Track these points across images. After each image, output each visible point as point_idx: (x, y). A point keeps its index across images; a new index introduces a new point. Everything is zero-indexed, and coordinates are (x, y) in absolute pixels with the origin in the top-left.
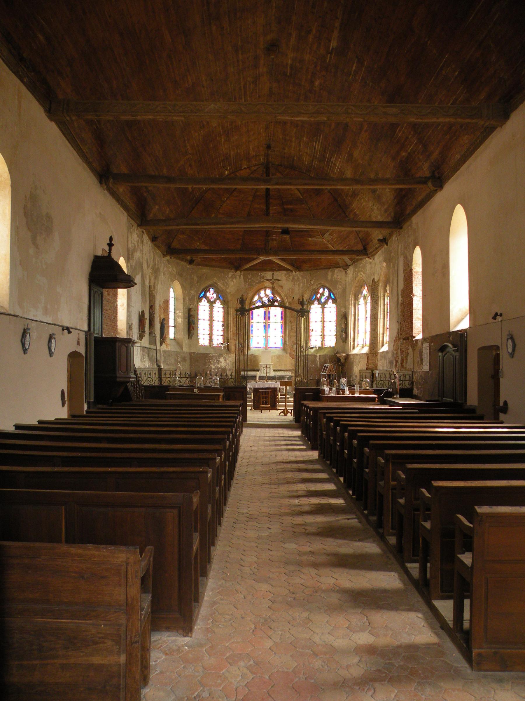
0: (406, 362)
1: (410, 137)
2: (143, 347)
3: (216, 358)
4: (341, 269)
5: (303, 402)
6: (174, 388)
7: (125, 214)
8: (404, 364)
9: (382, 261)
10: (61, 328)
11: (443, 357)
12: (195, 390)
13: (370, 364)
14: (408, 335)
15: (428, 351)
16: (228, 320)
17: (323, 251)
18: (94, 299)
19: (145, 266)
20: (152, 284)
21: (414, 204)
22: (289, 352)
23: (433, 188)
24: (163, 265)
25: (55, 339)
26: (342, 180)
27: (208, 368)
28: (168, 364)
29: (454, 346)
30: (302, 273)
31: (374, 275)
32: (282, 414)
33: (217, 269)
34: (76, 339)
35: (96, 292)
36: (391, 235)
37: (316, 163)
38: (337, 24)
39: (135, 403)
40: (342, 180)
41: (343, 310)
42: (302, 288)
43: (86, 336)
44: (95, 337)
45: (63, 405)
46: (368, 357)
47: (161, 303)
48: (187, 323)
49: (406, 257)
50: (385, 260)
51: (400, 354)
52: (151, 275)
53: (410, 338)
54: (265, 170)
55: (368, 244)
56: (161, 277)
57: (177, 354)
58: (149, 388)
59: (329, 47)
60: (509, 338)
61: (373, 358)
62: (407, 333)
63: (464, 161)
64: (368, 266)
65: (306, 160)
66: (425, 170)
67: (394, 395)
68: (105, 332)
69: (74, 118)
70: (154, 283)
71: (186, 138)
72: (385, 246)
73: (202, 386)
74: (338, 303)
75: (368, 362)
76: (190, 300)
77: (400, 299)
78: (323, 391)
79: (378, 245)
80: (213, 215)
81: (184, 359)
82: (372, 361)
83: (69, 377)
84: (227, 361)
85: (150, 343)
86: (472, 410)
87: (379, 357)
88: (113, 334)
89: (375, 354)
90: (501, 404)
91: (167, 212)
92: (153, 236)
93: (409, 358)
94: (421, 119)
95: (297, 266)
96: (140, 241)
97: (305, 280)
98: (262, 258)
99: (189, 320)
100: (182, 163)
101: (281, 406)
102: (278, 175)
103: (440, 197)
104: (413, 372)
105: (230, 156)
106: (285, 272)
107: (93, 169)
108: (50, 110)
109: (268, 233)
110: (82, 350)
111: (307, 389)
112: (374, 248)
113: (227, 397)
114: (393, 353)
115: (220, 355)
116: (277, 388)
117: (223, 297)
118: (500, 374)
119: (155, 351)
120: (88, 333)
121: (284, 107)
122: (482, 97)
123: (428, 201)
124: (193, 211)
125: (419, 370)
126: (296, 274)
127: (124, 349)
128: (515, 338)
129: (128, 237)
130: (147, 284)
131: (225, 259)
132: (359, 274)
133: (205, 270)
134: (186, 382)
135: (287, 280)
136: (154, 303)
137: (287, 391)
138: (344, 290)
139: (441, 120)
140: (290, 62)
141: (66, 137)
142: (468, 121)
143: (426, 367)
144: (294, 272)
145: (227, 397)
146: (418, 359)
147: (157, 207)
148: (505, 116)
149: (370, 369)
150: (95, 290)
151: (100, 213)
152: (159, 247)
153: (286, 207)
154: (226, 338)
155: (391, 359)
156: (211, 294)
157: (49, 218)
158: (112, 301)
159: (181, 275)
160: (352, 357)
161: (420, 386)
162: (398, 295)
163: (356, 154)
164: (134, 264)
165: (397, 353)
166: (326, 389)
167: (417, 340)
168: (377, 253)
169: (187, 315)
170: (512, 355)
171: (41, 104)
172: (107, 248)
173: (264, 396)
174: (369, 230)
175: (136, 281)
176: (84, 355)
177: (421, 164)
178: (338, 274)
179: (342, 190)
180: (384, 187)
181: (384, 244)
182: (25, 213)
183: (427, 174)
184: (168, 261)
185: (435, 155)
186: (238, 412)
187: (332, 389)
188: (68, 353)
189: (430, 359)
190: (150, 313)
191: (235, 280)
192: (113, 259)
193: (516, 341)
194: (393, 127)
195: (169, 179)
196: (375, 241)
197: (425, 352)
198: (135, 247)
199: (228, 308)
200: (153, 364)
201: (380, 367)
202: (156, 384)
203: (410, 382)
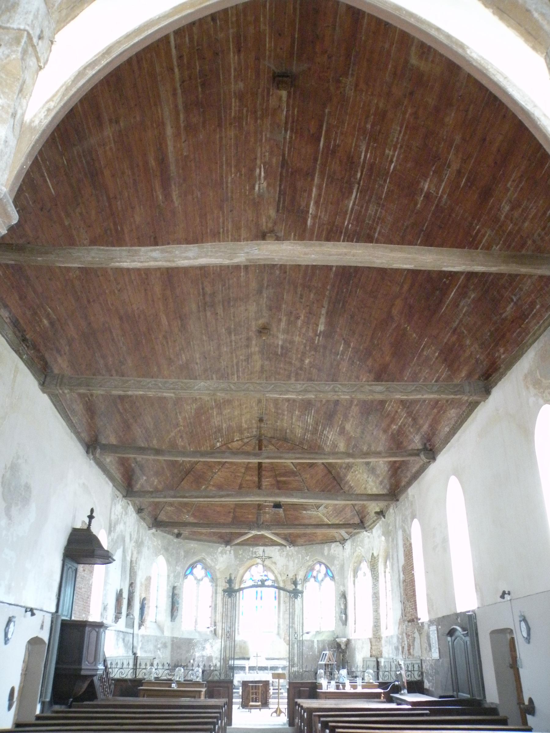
0: (413, 648)
1: (399, 410)
2: (118, 631)
3: (201, 644)
4: (338, 543)
5: (297, 700)
6: (150, 683)
7: (111, 484)
8: (411, 651)
9: (381, 535)
10: (24, 609)
11: (453, 642)
12: (174, 685)
13: (374, 651)
14: (413, 617)
15: (436, 635)
16: (216, 600)
17: (318, 525)
18: (67, 578)
19: (127, 539)
20: (134, 559)
21: (409, 476)
22: (283, 637)
23: (426, 460)
24: (148, 538)
25: (14, 622)
26: (334, 453)
27: (191, 655)
28: (145, 652)
29: (464, 629)
30: (296, 548)
31: (373, 550)
32: (275, 714)
33: (206, 543)
34: (40, 622)
35: (70, 567)
36: (388, 507)
37: (308, 436)
38: (324, 311)
39: (99, 703)
40: (334, 453)
41: (342, 588)
42: (297, 564)
43: (52, 618)
44: (63, 620)
45: (10, 708)
46: (371, 642)
47: (143, 580)
48: (170, 604)
49: (404, 531)
50: (384, 534)
51: (405, 638)
52: (133, 549)
53: (415, 620)
54: (257, 442)
55: (365, 516)
56: (145, 551)
57: (157, 639)
58: (120, 682)
59: (317, 331)
60: (521, 619)
61: (377, 644)
62: (412, 615)
63: (454, 434)
64: (366, 540)
65: (299, 432)
66: (416, 442)
67: (401, 690)
68: (75, 614)
69: (66, 391)
70: (137, 558)
71: (177, 411)
72: (383, 519)
73: (182, 680)
74: (336, 581)
75: (371, 648)
76: (175, 577)
77: (402, 575)
78: (320, 686)
79: (375, 518)
80: (203, 487)
81: (165, 646)
82: (376, 647)
83: (25, 669)
84: (214, 647)
85: (127, 626)
86: (493, 711)
87: (383, 642)
88: (84, 616)
89: (379, 638)
90: (526, 702)
91: (155, 483)
92: (139, 507)
93: (416, 644)
94: (407, 396)
95: (292, 541)
96: (124, 512)
97: (300, 556)
98: (254, 532)
99: (172, 599)
100: (173, 434)
101: (273, 704)
102: (271, 447)
103: (433, 469)
104: (421, 660)
105: (222, 429)
106: (278, 547)
107: (81, 440)
108: (44, 383)
109: (259, 507)
110: (45, 636)
111: (302, 683)
112: (371, 521)
113: (210, 694)
114: (398, 638)
115: (206, 640)
116: (269, 681)
117: (212, 575)
118: (519, 663)
119: (131, 636)
120: (55, 615)
121: (273, 386)
122: (463, 374)
123: (423, 472)
124: (183, 483)
125: (428, 658)
126: (291, 550)
127: (94, 634)
128: (527, 619)
129: (111, 509)
130: (128, 559)
131: (214, 533)
132: (357, 549)
133: (193, 545)
134: (163, 674)
135: (280, 555)
136: (135, 580)
137: (280, 684)
138: (342, 567)
139: (425, 396)
140: (280, 343)
141: (56, 408)
142: (452, 396)
143: (435, 655)
144: (288, 547)
145: (210, 694)
146: (425, 645)
147: (145, 478)
148: (487, 392)
149: (374, 656)
150: (70, 565)
151: (84, 484)
152: (144, 519)
153: (279, 479)
154: (213, 621)
155: (396, 645)
156: (199, 571)
157: (27, 487)
158: (87, 578)
159: (167, 550)
160: (353, 642)
161: (431, 678)
162: (399, 571)
163: (348, 427)
164: (115, 538)
165: (402, 638)
166: (323, 682)
167: (422, 623)
168: (374, 526)
169: (171, 594)
170: (528, 640)
171: (36, 378)
172: (87, 520)
173: (254, 691)
174: (365, 503)
175: (114, 558)
176: (47, 641)
177: (412, 436)
178: (335, 549)
179: (336, 463)
180: (377, 460)
181: (382, 517)
182: (2, 483)
183: (420, 446)
184: (153, 534)
185: (425, 427)
186: (218, 715)
187: (330, 683)
188: (28, 640)
189: (439, 645)
190: (129, 591)
191: (224, 556)
192: (92, 532)
193: (529, 622)
194: (382, 403)
195: (158, 452)
196: (372, 514)
197: (433, 637)
198: (118, 519)
199: (216, 586)
200: (128, 652)
201: (385, 654)
202: (130, 676)
203: (420, 673)
